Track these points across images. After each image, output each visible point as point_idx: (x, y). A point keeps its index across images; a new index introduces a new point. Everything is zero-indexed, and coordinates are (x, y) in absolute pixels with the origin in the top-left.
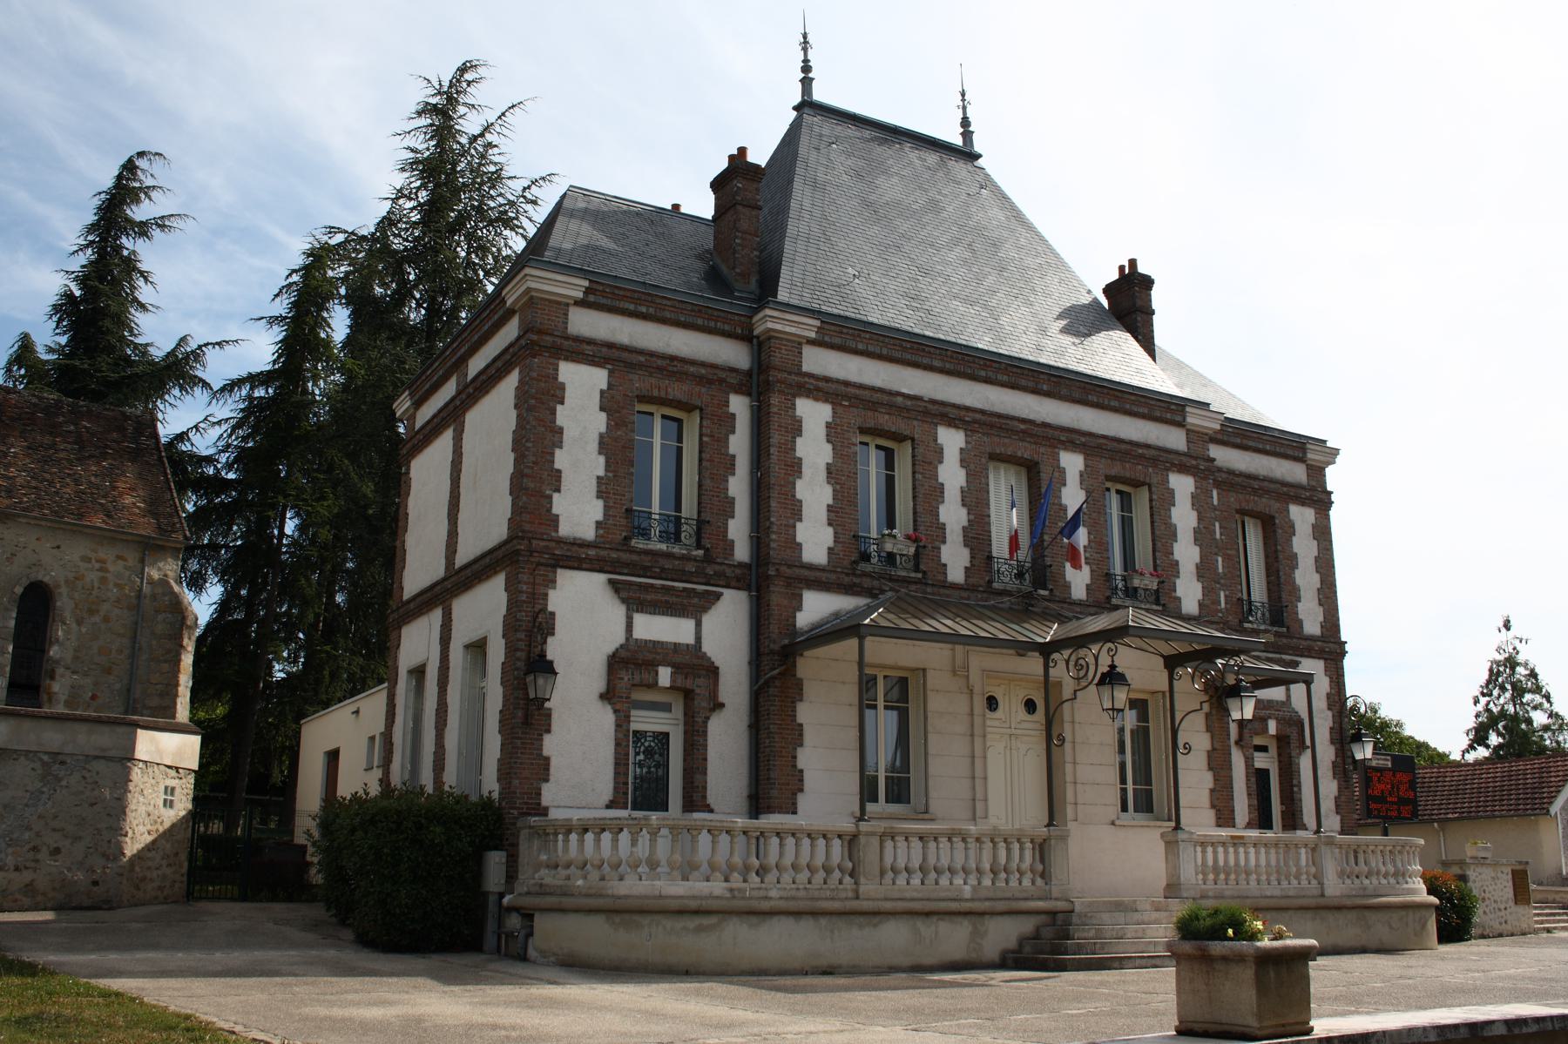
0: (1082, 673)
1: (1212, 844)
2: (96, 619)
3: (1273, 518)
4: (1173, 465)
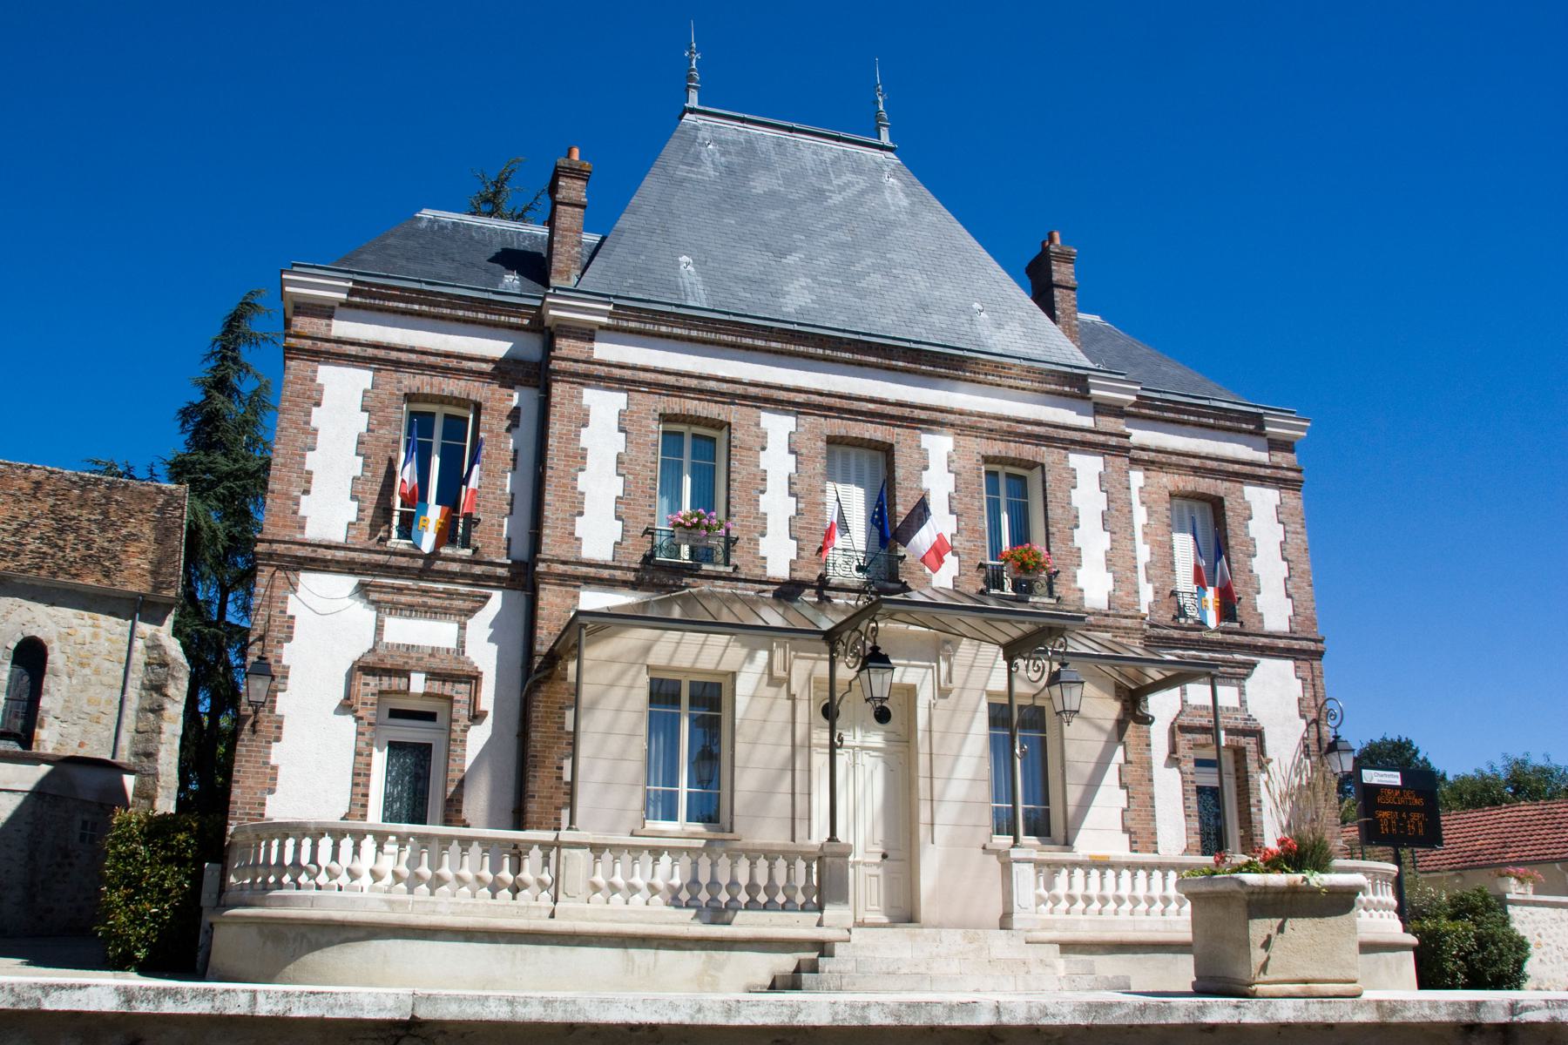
2: (87, 671)
3: (1221, 499)
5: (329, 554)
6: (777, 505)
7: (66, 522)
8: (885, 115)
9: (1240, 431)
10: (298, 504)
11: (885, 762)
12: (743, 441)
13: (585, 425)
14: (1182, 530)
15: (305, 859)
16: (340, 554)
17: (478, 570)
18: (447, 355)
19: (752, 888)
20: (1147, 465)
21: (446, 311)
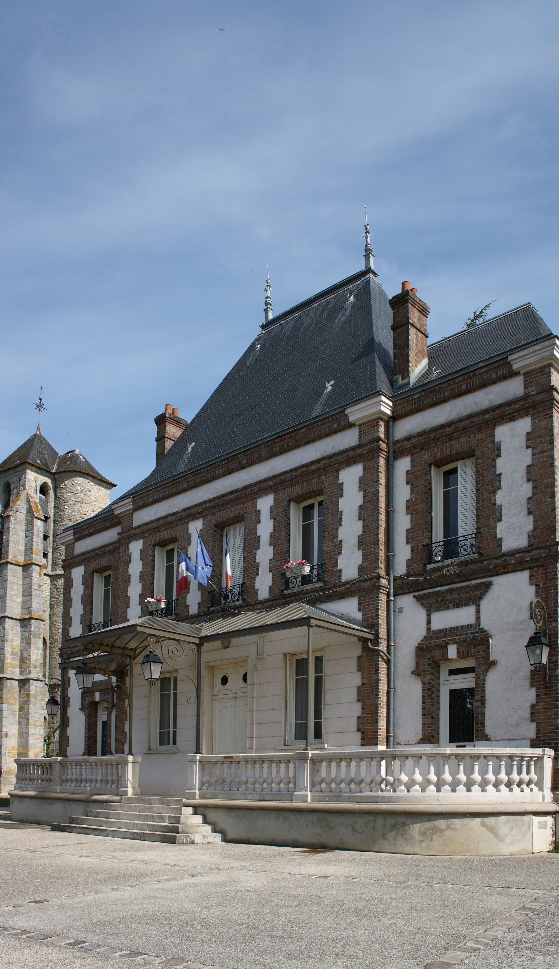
0: (541, 607)
4: (340, 463)
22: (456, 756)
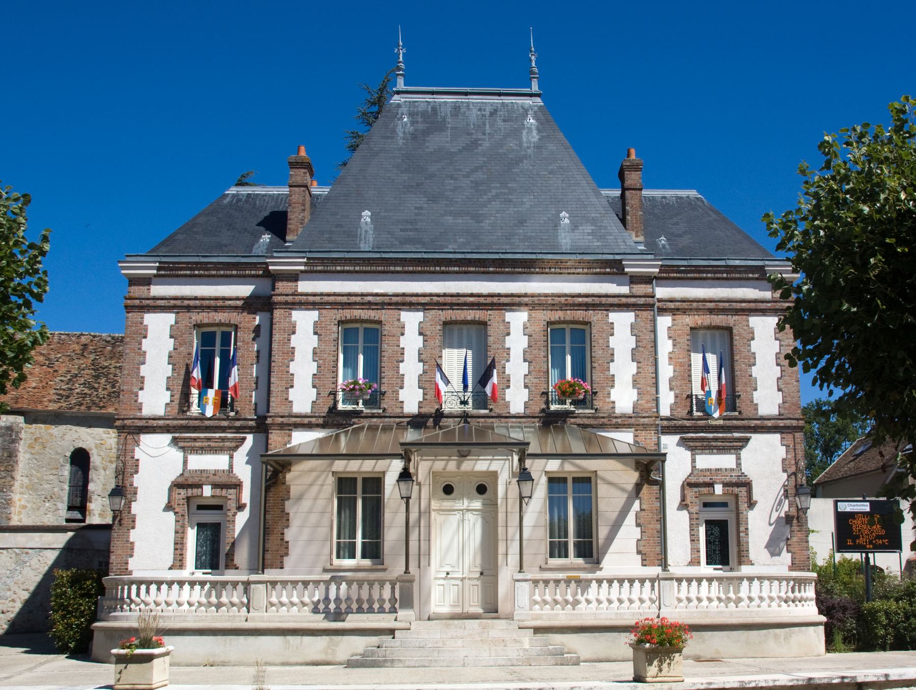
1: (786, 580)
5: (155, 423)
6: (411, 368)
7: (101, 371)
8: (536, 70)
9: (749, 279)
10: (137, 396)
11: (483, 518)
12: (389, 331)
13: (294, 333)
14: (696, 351)
15: (133, 596)
16: (161, 423)
17: (238, 424)
18: (217, 299)
19: (359, 601)
20: (674, 312)
21: (214, 272)
22: (728, 578)
